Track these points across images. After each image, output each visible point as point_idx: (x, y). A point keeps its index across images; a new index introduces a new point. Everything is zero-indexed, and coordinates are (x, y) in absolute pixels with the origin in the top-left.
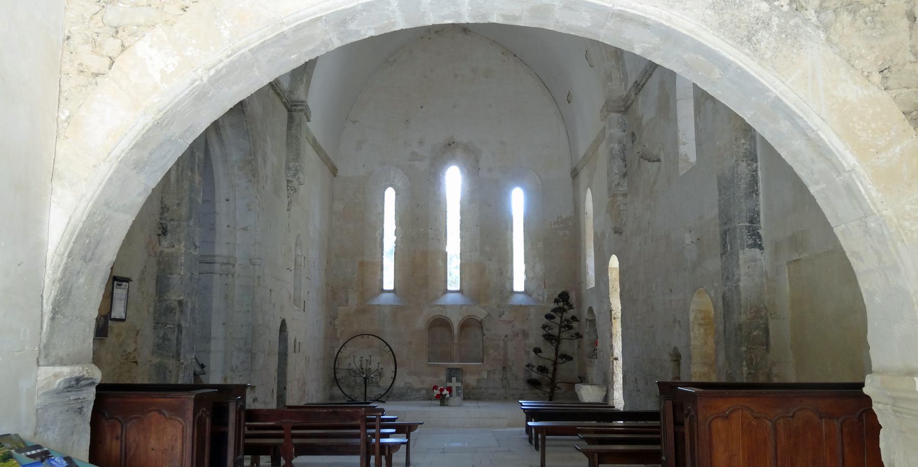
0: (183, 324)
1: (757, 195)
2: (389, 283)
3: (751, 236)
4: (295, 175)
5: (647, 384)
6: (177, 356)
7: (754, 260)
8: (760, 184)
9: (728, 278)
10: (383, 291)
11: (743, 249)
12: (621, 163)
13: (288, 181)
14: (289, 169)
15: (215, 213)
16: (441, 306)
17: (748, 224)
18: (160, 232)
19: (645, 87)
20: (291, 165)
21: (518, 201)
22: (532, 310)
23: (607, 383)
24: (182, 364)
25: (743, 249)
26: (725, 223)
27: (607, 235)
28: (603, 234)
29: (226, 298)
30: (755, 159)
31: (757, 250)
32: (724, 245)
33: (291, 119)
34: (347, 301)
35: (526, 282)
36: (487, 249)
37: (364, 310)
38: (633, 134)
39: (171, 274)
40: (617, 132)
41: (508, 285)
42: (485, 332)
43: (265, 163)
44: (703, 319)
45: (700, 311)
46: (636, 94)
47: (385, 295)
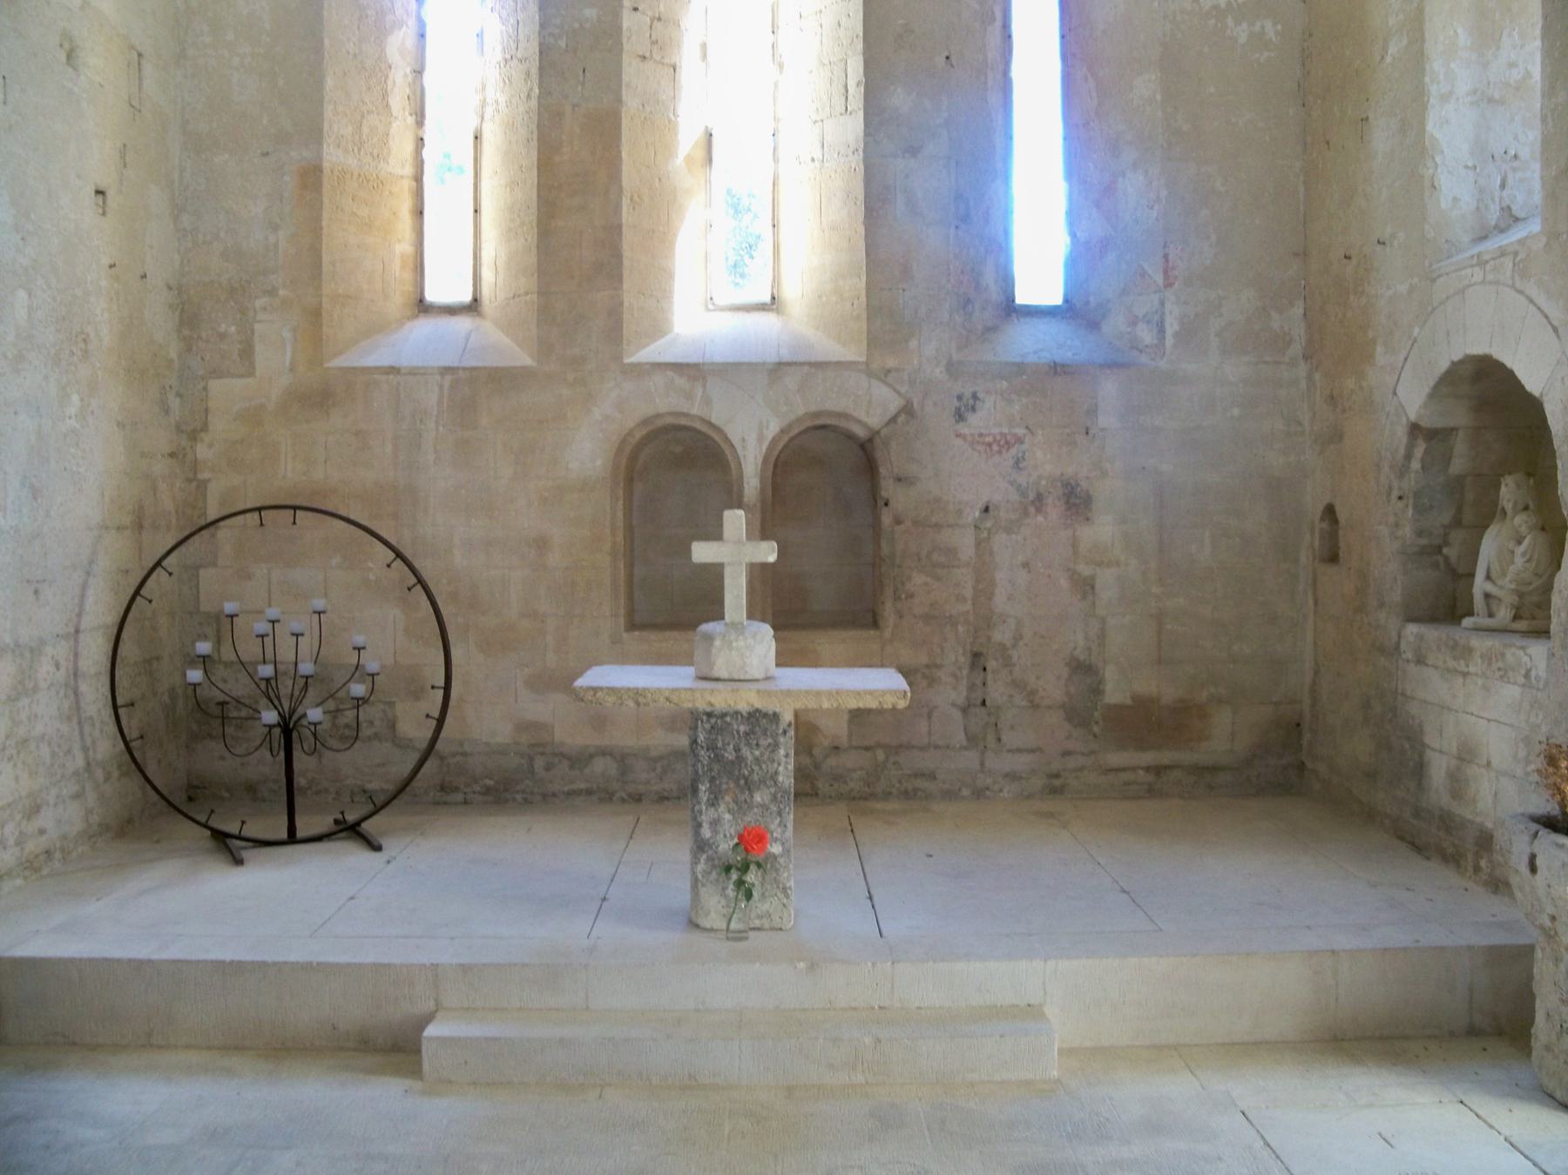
34: (247, 352)
35: (1083, 259)
41: (989, 278)
42: (888, 489)
47: (424, 328)
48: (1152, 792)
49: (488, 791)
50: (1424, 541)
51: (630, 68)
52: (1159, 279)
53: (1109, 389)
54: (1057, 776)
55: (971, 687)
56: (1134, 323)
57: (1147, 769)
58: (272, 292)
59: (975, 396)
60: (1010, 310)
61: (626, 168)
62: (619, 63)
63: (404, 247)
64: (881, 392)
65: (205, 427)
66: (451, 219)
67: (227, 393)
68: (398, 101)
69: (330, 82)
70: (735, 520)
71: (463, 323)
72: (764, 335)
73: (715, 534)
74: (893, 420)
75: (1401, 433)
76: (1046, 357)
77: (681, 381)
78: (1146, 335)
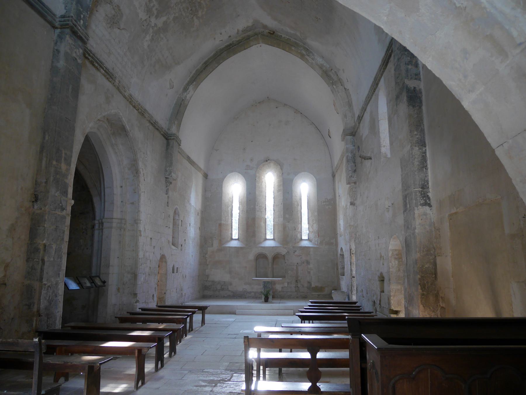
0: (46, 259)
1: (427, 169)
2: (235, 235)
3: (423, 197)
4: (169, 174)
6: (41, 279)
7: (425, 214)
8: (429, 162)
9: (408, 227)
10: (232, 239)
11: (417, 207)
12: (353, 164)
13: (166, 178)
14: (166, 171)
15: (114, 194)
16: (262, 247)
17: (420, 189)
18: (34, 200)
21: (305, 189)
22: (312, 249)
24: (45, 285)
25: (417, 207)
26: (406, 190)
29: (120, 242)
30: (424, 145)
31: (427, 207)
32: (405, 205)
33: (168, 145)
34: (212, 245)
36: (287, 216)
37: (222, 249)
38: (359, 147)
39: (39, 226)
40: (351, 147)
41: (299, 235)
42: (286, 261)
44: (397, 255)
45: (396, 250)
46: (359, 123)
67: (210, 249)
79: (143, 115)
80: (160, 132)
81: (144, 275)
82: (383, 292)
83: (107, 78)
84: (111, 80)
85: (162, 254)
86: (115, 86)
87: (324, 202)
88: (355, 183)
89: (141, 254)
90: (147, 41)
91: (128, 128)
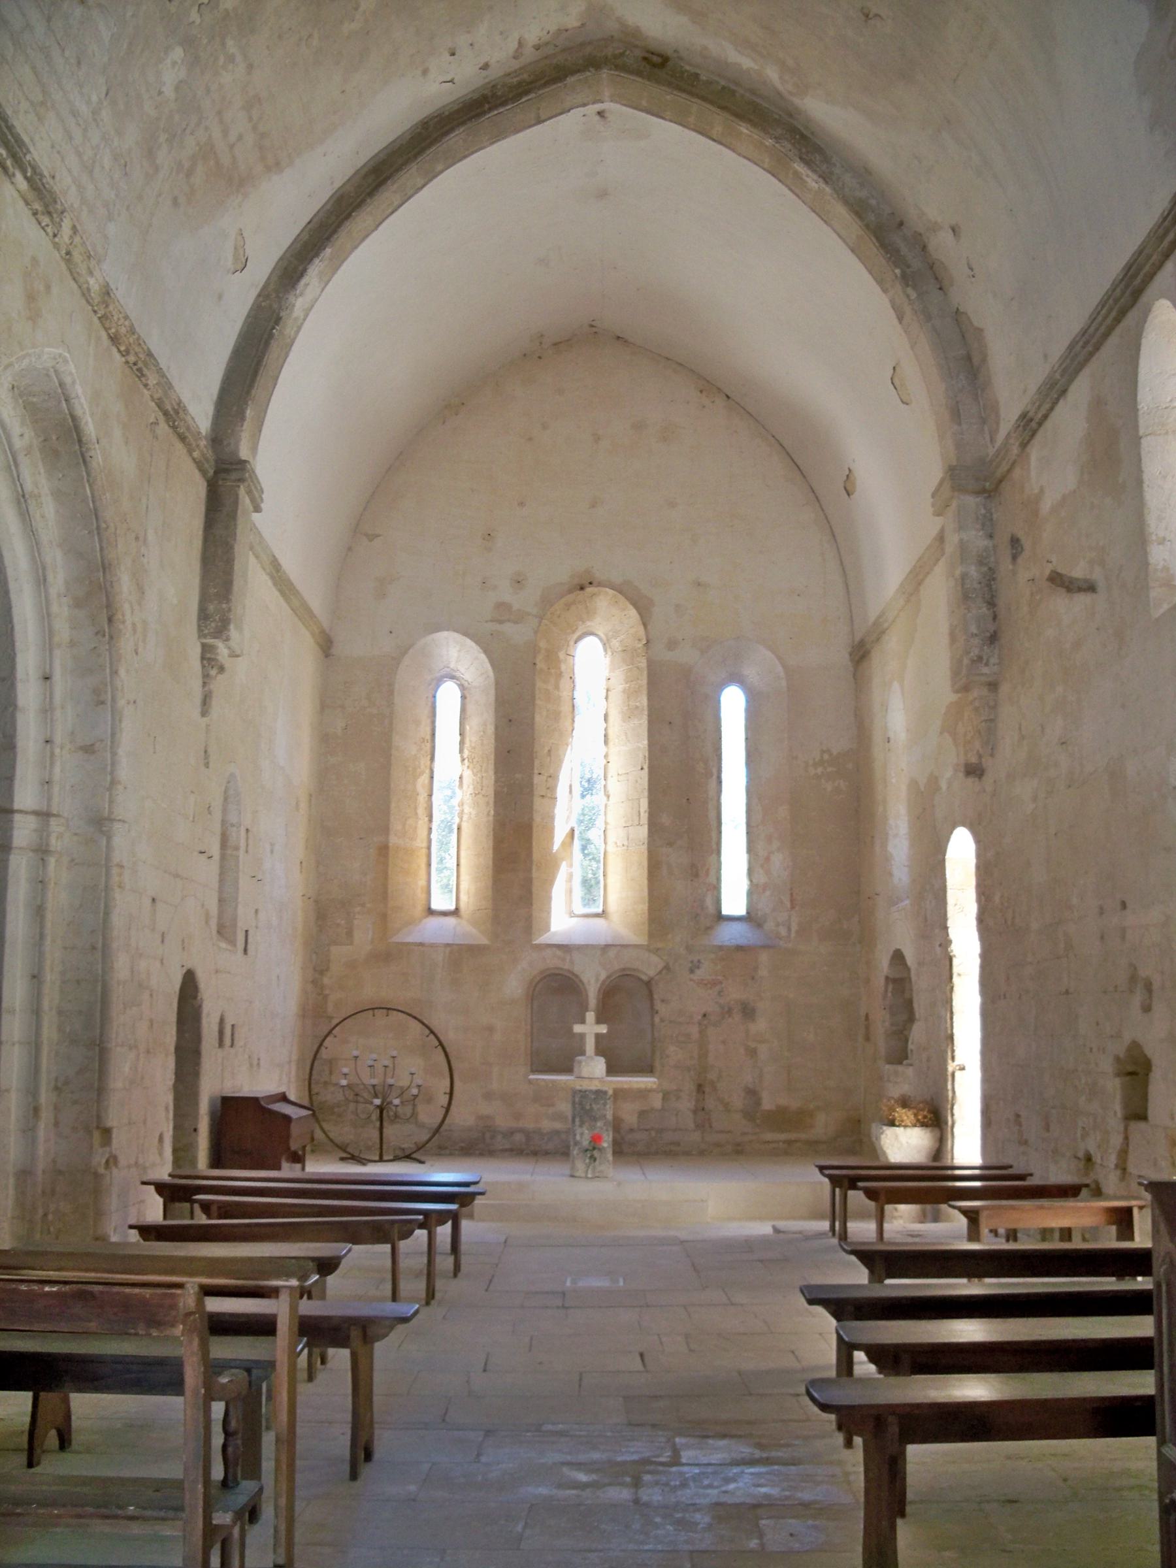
5: (1047, 1128)
19: (1048, 424)
20: (211, 608)
23: (936, 1117)
27: (944, 786)
28: (933, 781)
34: (350, 933)
35: (753, 893)
40: (978, 541)
41: (709, 902)
42: (658, 1005)
43: (141, 590)
46: (1024, 445)
47: (433, 922)
48: (786, 1153)
49: (462, 1149)
50: (894, 1028)
51: (537, 802)
52: (788, 904)
53: (764, 957)
54: (739, 1145)
55: (697, 1101)
56: (778, 925)
57: (784, 1142)
58: (363, 905)
59: (699, 961)
60: (720, 917)
61: (535, 850)
62: (532, 802)
63: (422, 882)
64: (654, 959)
65: (328, 969)
66: (448, 874)
67: (339, 953)
68: (421, 811)
69: (393, 805)
70: (590, 1016)
71: (451, 921)
72: (600, 931)
73: (583, 1022)
74: (660, 972)
75: (882, 981)
76: (734, 942)
77: (559, 953)
78: (783, 931)
79: (141, 374)
80: (190, 452)
81: (132, 1055)
82: (1142, 1116)
83: (35, 214)
84: (46, 220)
85: (189, 965)
86: (56, 246)
87: (815, 765)
88: (993, 686)
89: (121, 965)
90: (174, 63)
91: (90, 428)
